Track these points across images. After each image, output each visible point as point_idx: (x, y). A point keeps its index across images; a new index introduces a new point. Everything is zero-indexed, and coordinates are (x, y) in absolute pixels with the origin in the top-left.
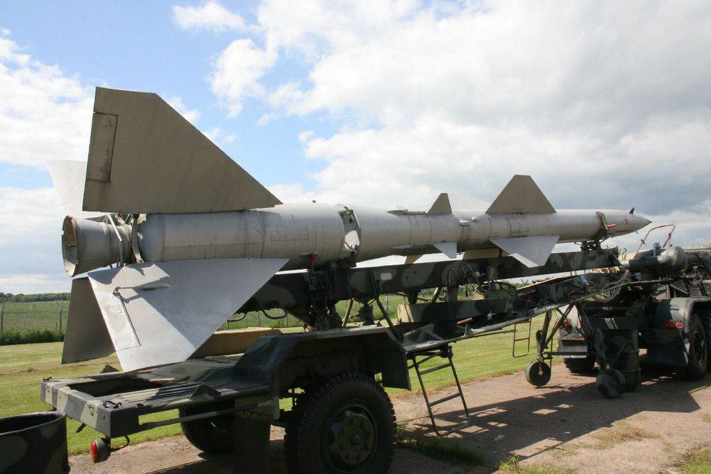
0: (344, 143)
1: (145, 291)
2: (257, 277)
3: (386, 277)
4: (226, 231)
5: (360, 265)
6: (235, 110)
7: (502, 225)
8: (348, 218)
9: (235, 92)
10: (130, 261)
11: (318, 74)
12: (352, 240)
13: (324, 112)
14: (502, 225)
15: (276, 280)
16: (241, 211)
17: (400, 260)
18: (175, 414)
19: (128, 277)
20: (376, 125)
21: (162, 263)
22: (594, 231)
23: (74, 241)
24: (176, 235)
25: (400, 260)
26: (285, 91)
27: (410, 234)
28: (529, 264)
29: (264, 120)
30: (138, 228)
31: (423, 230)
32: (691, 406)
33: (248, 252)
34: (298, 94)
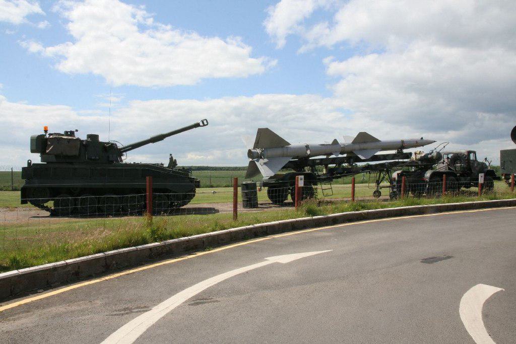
0: (357, 63)
1: (265, 164)
2: (285, 161)
3: (318, 161)
4: (279, 151)
5: (310, 158)
6: (281, 43)
7: (357, 146)
8: (307, 147)
9: (282, 32)
10: (261, 158)
11: (339, 16)
12: (309, 152)
13: (344, 43)
14: (357, 146)
15: (290, 162)
16: (282, 147)
17: (325, 157)
18: (259, 206)
19: (261, 161)
20: (381, 50)
21: (267, 158)
22: (399, 146)
23: (250, 154)
24: (270, 153)
25: (325, 157)
26: (319, 29)
27: (326, 150)
28: (362, 158)
29: (302, 50)
30: (262, 151)
31: (328, 150)
32: (40, 143)
33: (283, 156)
34: (327, 31)
